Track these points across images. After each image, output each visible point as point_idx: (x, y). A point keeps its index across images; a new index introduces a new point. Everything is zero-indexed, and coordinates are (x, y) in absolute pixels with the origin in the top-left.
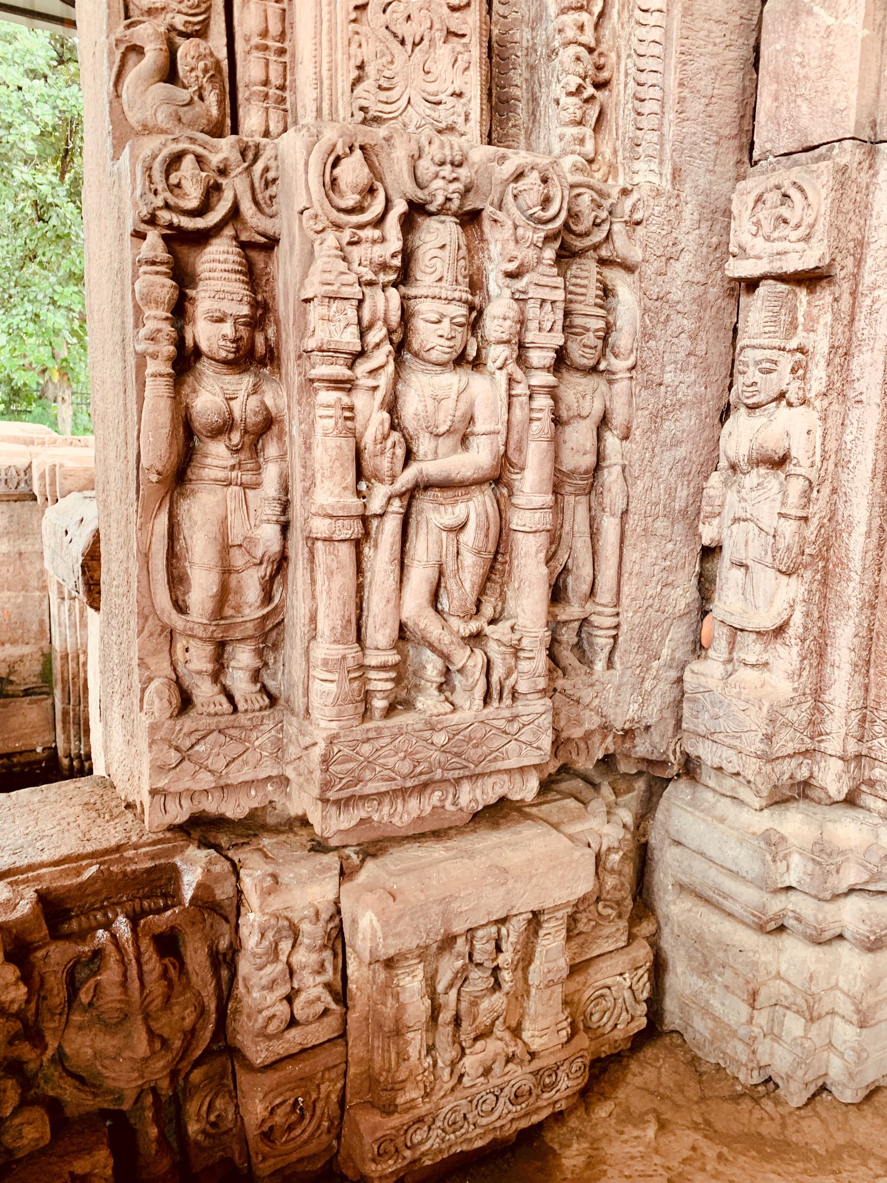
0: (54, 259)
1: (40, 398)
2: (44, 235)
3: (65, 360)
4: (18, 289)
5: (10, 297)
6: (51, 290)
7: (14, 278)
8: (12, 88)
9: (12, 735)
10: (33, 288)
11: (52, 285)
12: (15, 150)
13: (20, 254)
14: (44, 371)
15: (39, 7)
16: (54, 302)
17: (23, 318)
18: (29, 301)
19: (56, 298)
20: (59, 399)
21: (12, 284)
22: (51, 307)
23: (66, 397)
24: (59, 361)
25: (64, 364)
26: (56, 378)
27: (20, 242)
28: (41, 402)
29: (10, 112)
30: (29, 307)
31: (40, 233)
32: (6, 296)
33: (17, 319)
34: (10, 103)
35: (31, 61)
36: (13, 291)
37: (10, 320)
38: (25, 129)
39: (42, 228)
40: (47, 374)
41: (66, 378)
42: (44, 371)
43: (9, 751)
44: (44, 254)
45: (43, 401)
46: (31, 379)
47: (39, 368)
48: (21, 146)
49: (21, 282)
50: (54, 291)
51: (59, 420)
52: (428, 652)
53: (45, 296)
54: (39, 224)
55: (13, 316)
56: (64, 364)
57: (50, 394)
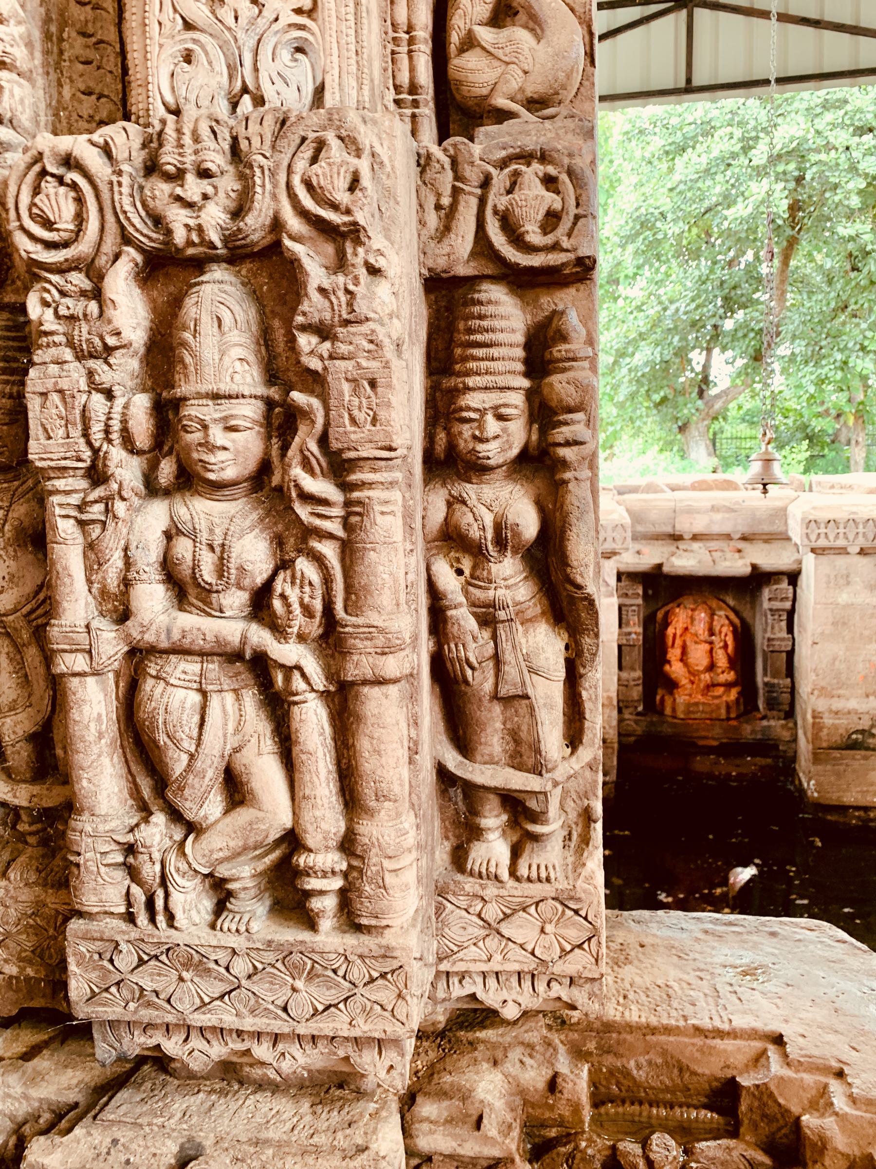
0: (866, 305)
1: (833, 442)
2: (858, 284)
3: (862, 403)
4: (829, 340)
5: (821, 348)
6: (861, 336)
7: (826, 330)
8: (840, 150)
9: (871, 789)
10: (844, 337)
11: (863, 332)
12: (840, 208)
13: (833, 305)
14: (839, 416)
15: (829, 16)
16: (863, 348)
17: (832, 367)
18: (839, 350)
19: (866, 343)
20: (853, 442)
21: (824, 336)
22: (861, 354)
23: (860, 439)
24: (855, 404)
25: (861, 407)
26: (851, 421)
27: (833, 294)
28: (834, 446)
29: (837, 174)
30: (839, 356)
31: (853, 283)
32: (817, 348)
33: (827, 369)
34: (838, 164)
35: (860, 119)
36: (823, 343)
37: (819, 371)
38: (851, 186)
39: (855, 278)
40: (842, 419)
41: (860, 421)
42: (839, 416)
43: (868, 804)
44: (856, 303)
45: (836, 445)
46: (826, 425)
47: (833, 412)
48: (846, 203)
49: (832, 333)
50: (865, 337)
51: (852, 462)
52: (490, 272)
53: (855, 344)
54: (853, 275)
55: (822, 367)
56: (861, 407)
57: (843, 438)
